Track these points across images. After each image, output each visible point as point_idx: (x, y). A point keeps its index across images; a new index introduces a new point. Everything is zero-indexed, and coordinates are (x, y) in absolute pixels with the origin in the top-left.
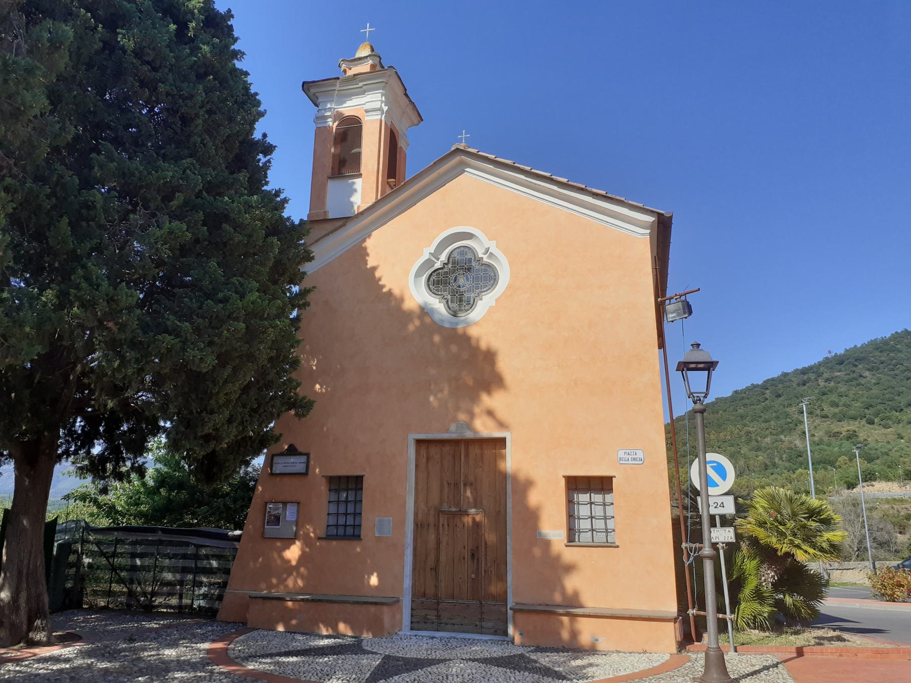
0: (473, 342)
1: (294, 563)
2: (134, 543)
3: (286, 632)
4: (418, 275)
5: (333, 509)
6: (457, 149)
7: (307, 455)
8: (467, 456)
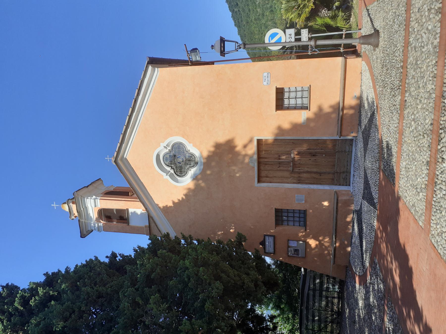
0: (211, 154)
1: (317, 243)
2: (308, 320)
4: (177, 181)
5: (291, 223)
7: (265, 236)
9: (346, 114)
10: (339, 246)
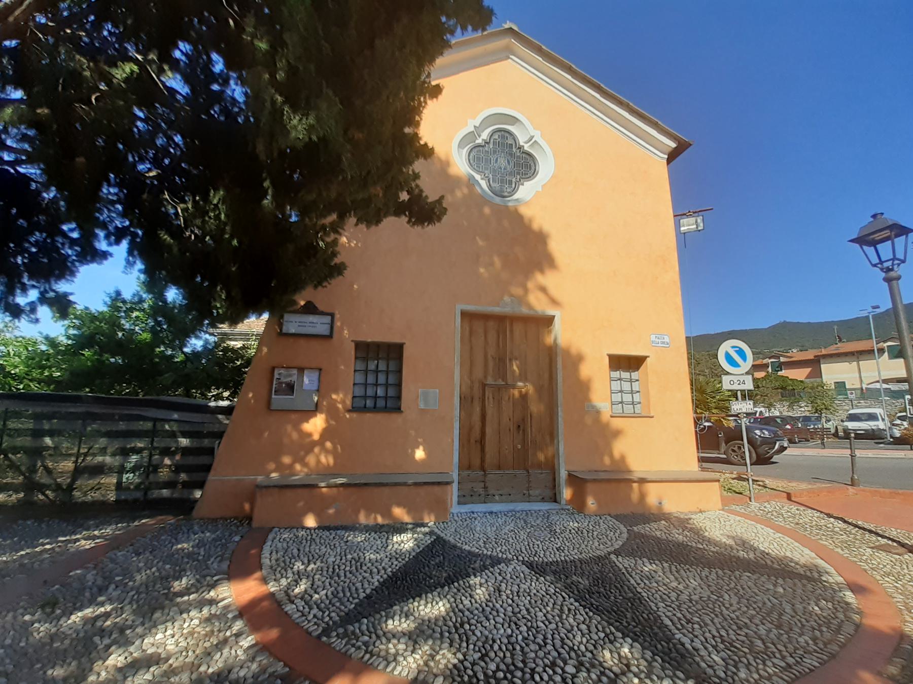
0: (526, 221)
1: (316, 437)
2: (37, 417)
3: (319, 528)
4: (461, 145)
5: (360, 378)
6: (511, 28)
7: (332, 315)
8: (512, 331)
10: (322, 494)
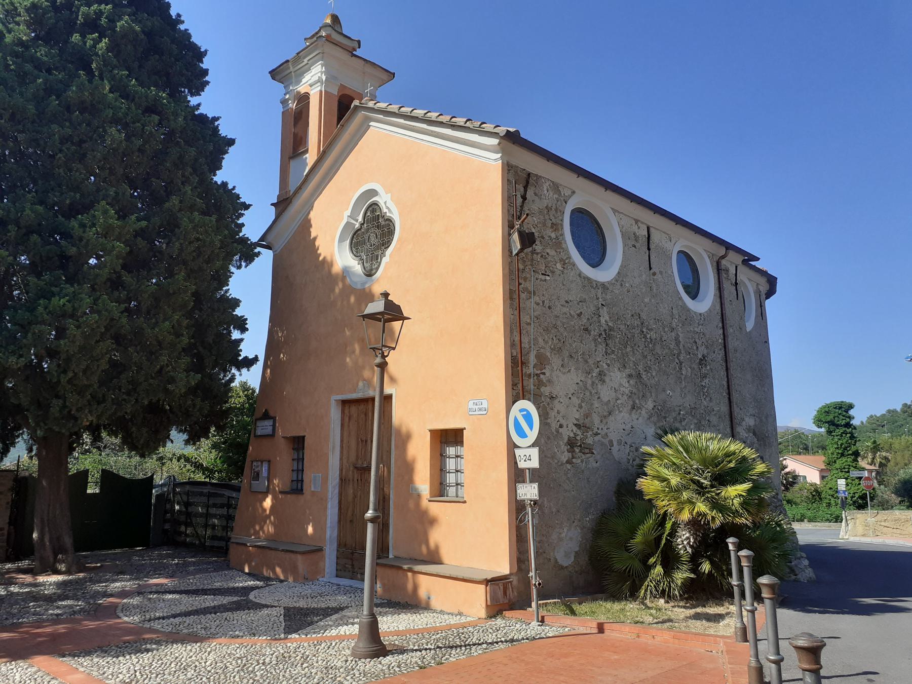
4: (341, 240)
9: (407, 576)
